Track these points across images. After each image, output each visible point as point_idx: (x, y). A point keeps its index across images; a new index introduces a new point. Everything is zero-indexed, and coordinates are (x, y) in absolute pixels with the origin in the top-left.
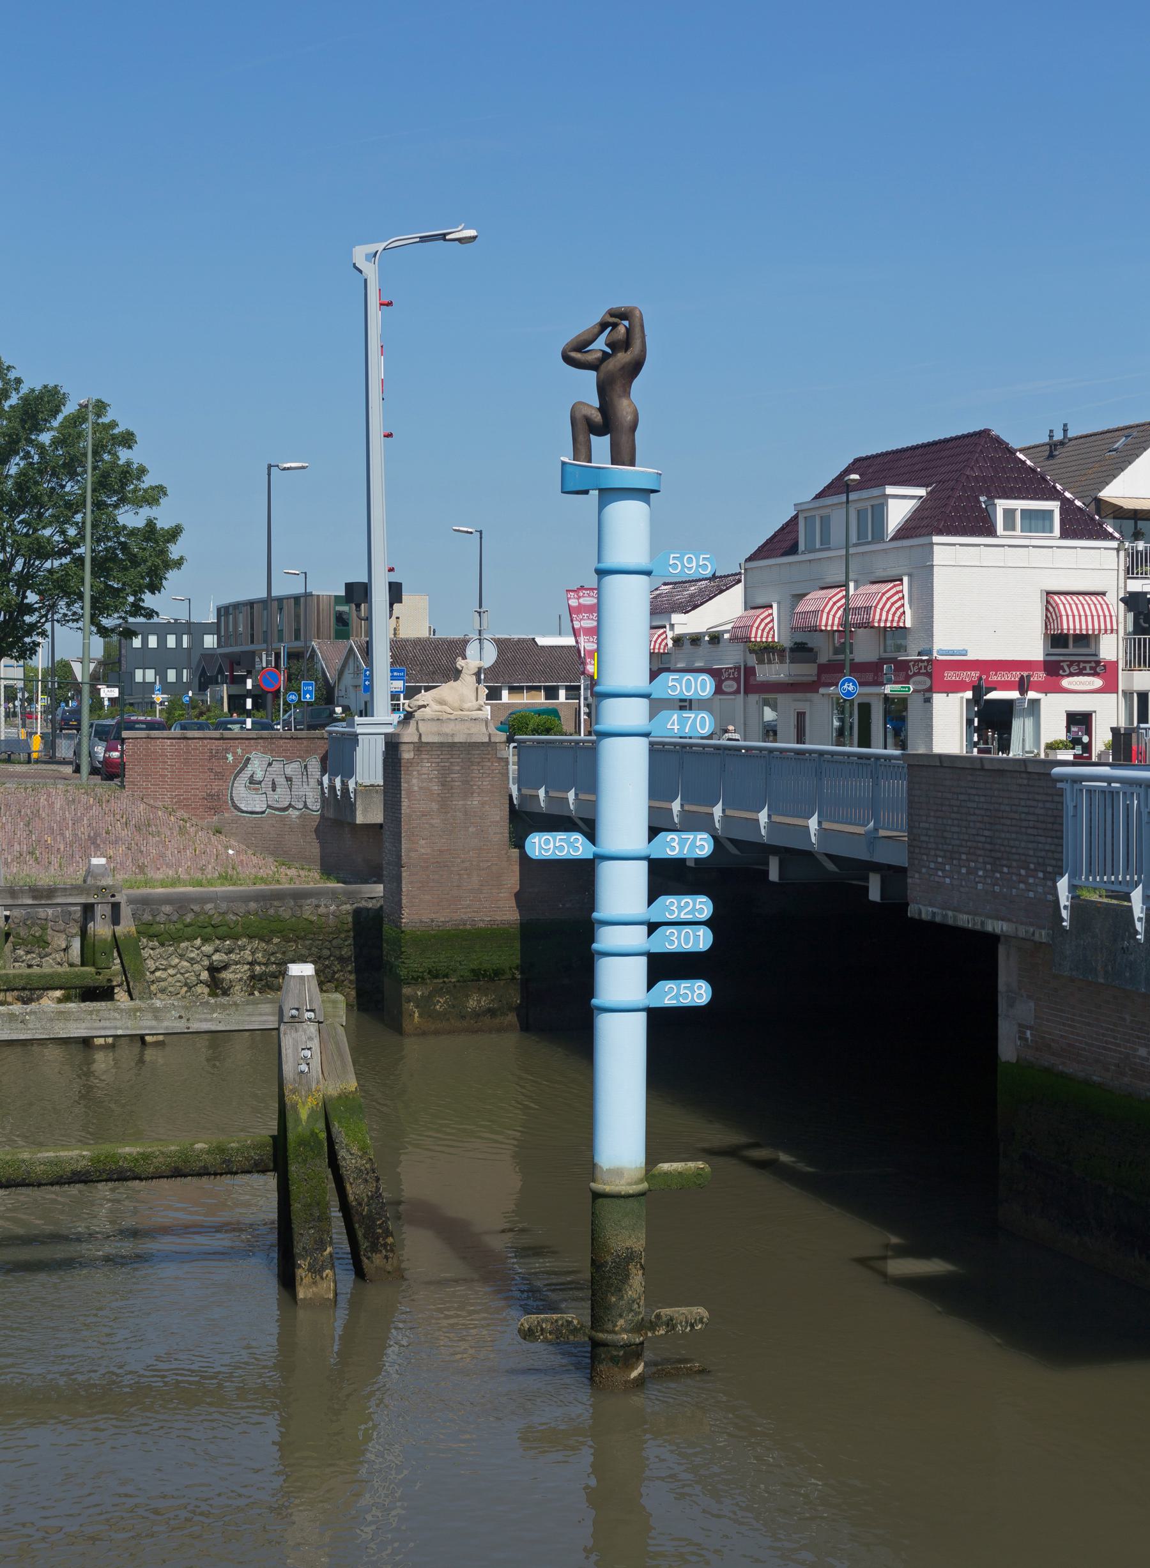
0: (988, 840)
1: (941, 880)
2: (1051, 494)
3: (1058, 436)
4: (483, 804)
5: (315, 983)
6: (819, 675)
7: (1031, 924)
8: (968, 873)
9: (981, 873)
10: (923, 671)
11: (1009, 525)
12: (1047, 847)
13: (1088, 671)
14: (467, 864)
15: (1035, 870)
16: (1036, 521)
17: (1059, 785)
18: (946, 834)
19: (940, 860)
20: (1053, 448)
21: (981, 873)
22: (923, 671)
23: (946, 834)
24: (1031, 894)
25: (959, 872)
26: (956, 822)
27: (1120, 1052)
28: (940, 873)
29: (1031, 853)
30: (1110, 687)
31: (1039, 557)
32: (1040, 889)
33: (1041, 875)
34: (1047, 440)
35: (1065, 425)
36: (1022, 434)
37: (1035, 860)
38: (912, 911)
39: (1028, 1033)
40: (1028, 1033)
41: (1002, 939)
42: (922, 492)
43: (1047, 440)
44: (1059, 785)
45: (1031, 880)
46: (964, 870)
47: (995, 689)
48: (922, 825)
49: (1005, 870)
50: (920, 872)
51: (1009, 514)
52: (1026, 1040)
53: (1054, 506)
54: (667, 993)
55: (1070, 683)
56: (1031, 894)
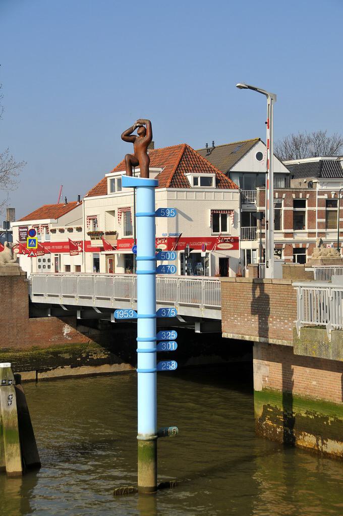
0: (256, 308)
1: (236, 323)
2: (210, 170)
3: (210, 146)
4: (18, 300)
5: (10, 370)
6: (118, 244)
7: (275, 338)
8: (248, 321)
9: (253, 320)
10: (163, 242)
11: (196, 183)
12: (281, 310)
13: (227, 241)
14: (12, 325)
15: (276, 319)
16: (206, 182)
17: (295, 288)
18: (238, 307)
19: (235, 316)
20: (209, 151)
21: (253, 320)
22: (163, 242)
23: (238, 307)
24: (275, 327)
25: (244, 320)
26: (242, 302)
27: (305, 384)
28: (236, 321)
29: (274, 312)
30: (236, 247)
31: (211, 196)
32: (278, 326)
33: (279, 320)
34: (205, 147)
35: (207, 144)
36: (197, 145)
37: (276, 315)
38: (224, 335)
39: (267, 379)
40: (267, 379)
41: (254, 344)
42: (160, 169)
43: (205, 147)
44: (295, 288)
45: (274, 322)
46: (246, 320)
47: (194, 249)
48: (227, 304)
49: (264, 319)
50: (227, 321)
51: (195, 180)
52: (266, 381)
53: (213, 175)
54: (162, 366)
55: (220, 246)
56: (275, 327)
